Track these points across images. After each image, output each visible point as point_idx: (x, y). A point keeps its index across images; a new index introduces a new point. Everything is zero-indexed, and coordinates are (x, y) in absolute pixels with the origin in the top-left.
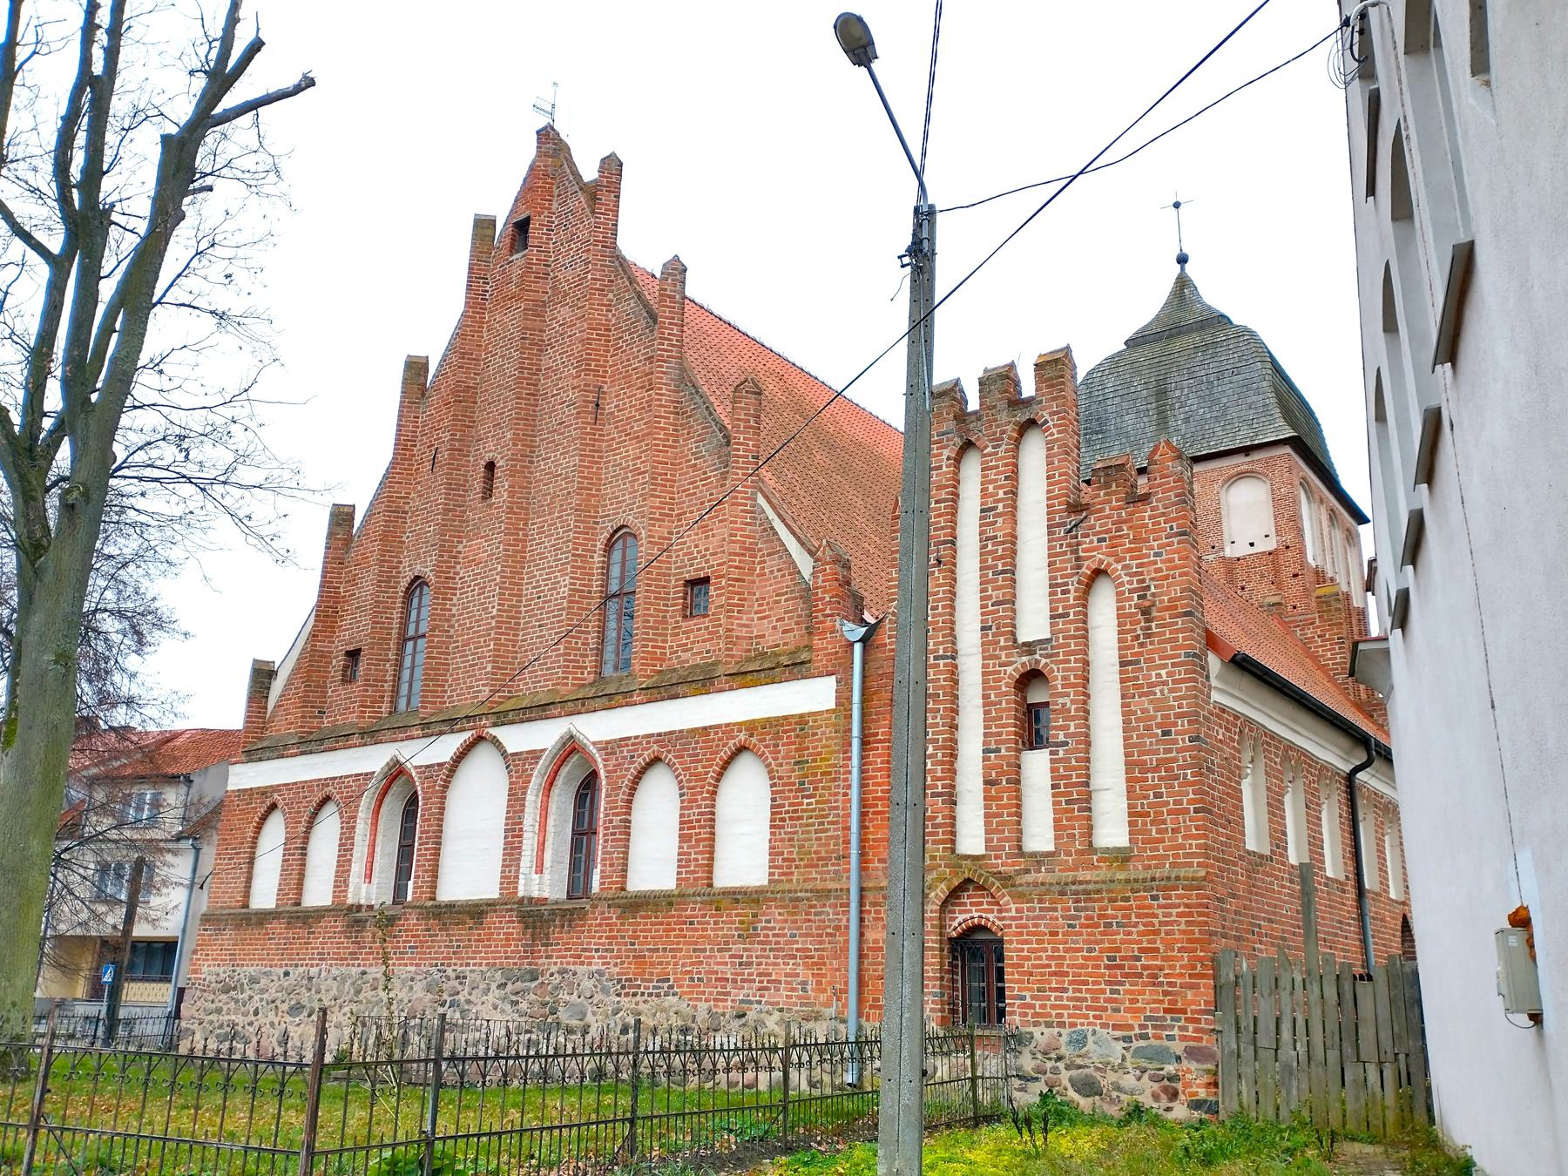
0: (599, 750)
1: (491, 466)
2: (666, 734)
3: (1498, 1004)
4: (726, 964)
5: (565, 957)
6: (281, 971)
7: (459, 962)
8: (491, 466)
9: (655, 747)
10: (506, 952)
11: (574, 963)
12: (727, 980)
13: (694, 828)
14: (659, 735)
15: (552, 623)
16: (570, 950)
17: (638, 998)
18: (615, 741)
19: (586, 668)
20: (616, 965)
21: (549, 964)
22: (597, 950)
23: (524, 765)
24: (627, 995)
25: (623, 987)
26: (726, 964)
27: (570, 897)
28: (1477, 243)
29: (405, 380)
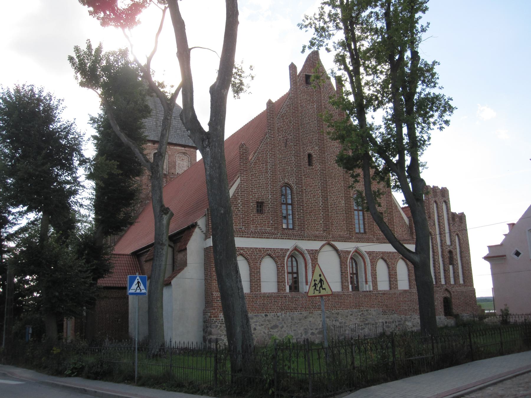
0: (367, 253)
1: (310, 156)
2: (384, 252)
3: (436, 185)
4: (406, 306)
5: (367, 306)
6: (263, 315)
7: (336, 309)
8: (310, 156)
9: (382, 255)
10: (350, 306)
11: (370, 308)
12: (407, 310)
13: (393, 276)
14: (382, 252)
15: (340, 213)
16: (368, 305)
17: (388, 315)
18: (371, 252)
19: (297, 204)
20: (381, 308)
21: (363, 308)
22: (376, 305)
23: (345, 254)
24: (385, 315)
25: (384, 313)
26: (406, 306)
27: (390, 289)
28: (488, 245)
29: (471, 270)
